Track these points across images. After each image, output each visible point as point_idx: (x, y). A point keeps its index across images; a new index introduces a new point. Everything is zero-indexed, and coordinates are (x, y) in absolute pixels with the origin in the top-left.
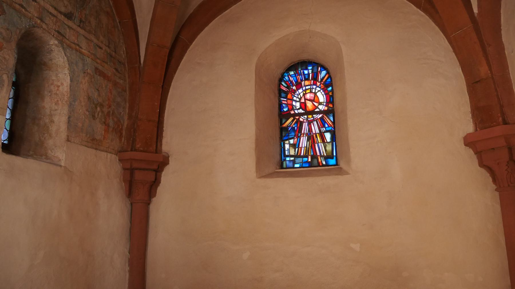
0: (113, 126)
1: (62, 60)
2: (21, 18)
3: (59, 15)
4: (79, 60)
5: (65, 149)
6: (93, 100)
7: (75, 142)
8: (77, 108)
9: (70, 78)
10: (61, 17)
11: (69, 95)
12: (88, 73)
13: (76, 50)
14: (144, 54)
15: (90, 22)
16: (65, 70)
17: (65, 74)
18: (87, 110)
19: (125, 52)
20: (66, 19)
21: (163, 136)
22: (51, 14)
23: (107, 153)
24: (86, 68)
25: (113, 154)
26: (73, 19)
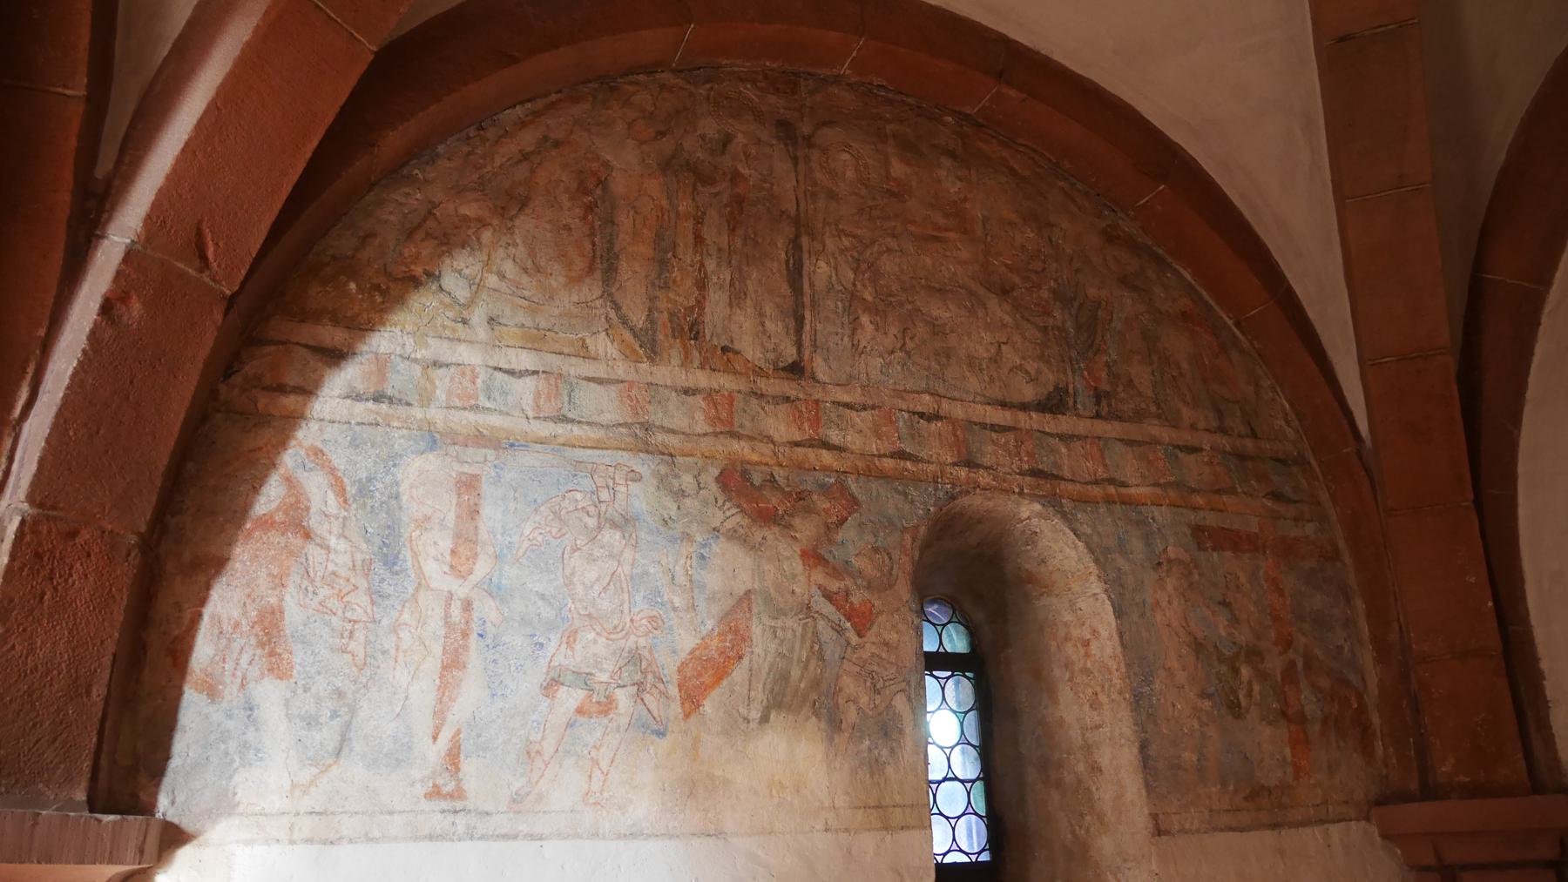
0: (1319, 712)
1: (1073, 553)
2: (905, 494)
3: (1022, 416)
4: (1127, 532)
5: (1154, 867)
6: (1216, 646)
7: (1187, 826)
8: (1162, 701)
9: (1113, 606)
10: (1031, 418)
11: (1123, 669)
12: (1169, 561)
13: (1109, 501)
14: (1362, 397)
15: (1130, 383)
16: (1092, 583)
17: (1094, 594)
18: (1203, 695)
19: (1292, 416)
21: (1549, 699)
22: (996, 431)
23: (1327, 826)
24: (1161, 547)
25: (1351, 820)
26: (1071, 403)
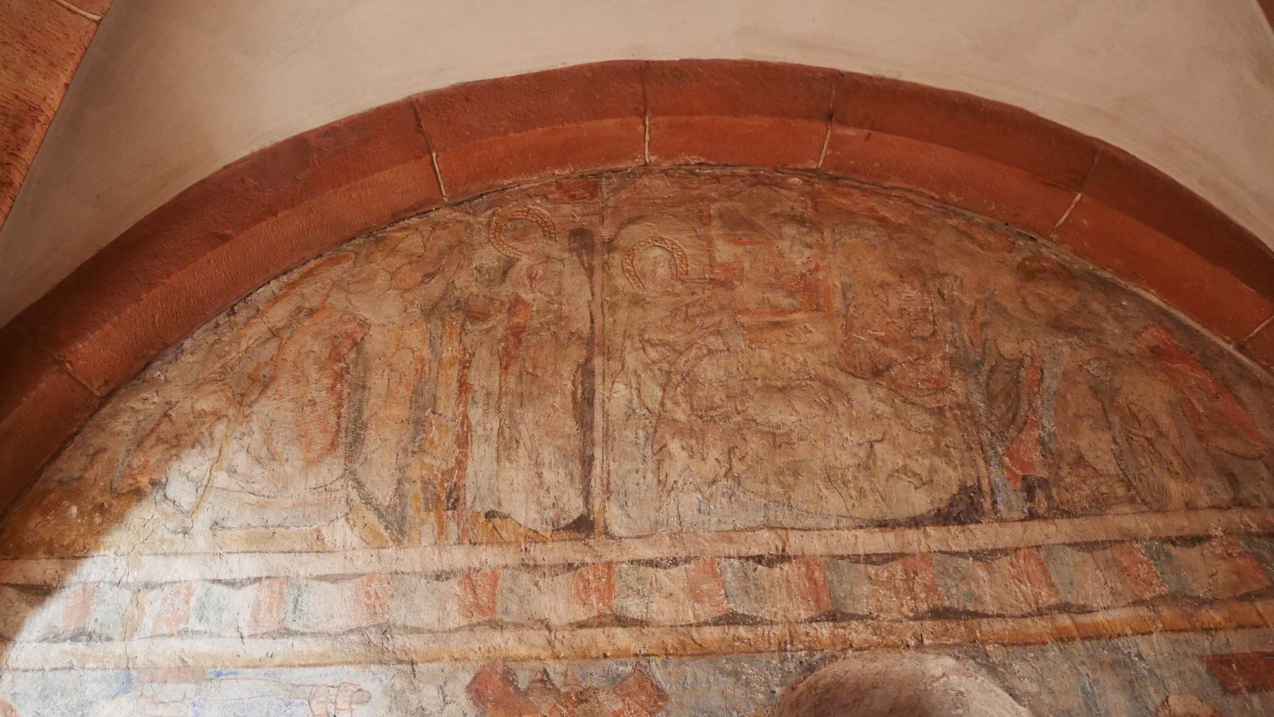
3: (912, 535)
13: (1062, 638)
20: (954, 529)
22: (874, 563)
